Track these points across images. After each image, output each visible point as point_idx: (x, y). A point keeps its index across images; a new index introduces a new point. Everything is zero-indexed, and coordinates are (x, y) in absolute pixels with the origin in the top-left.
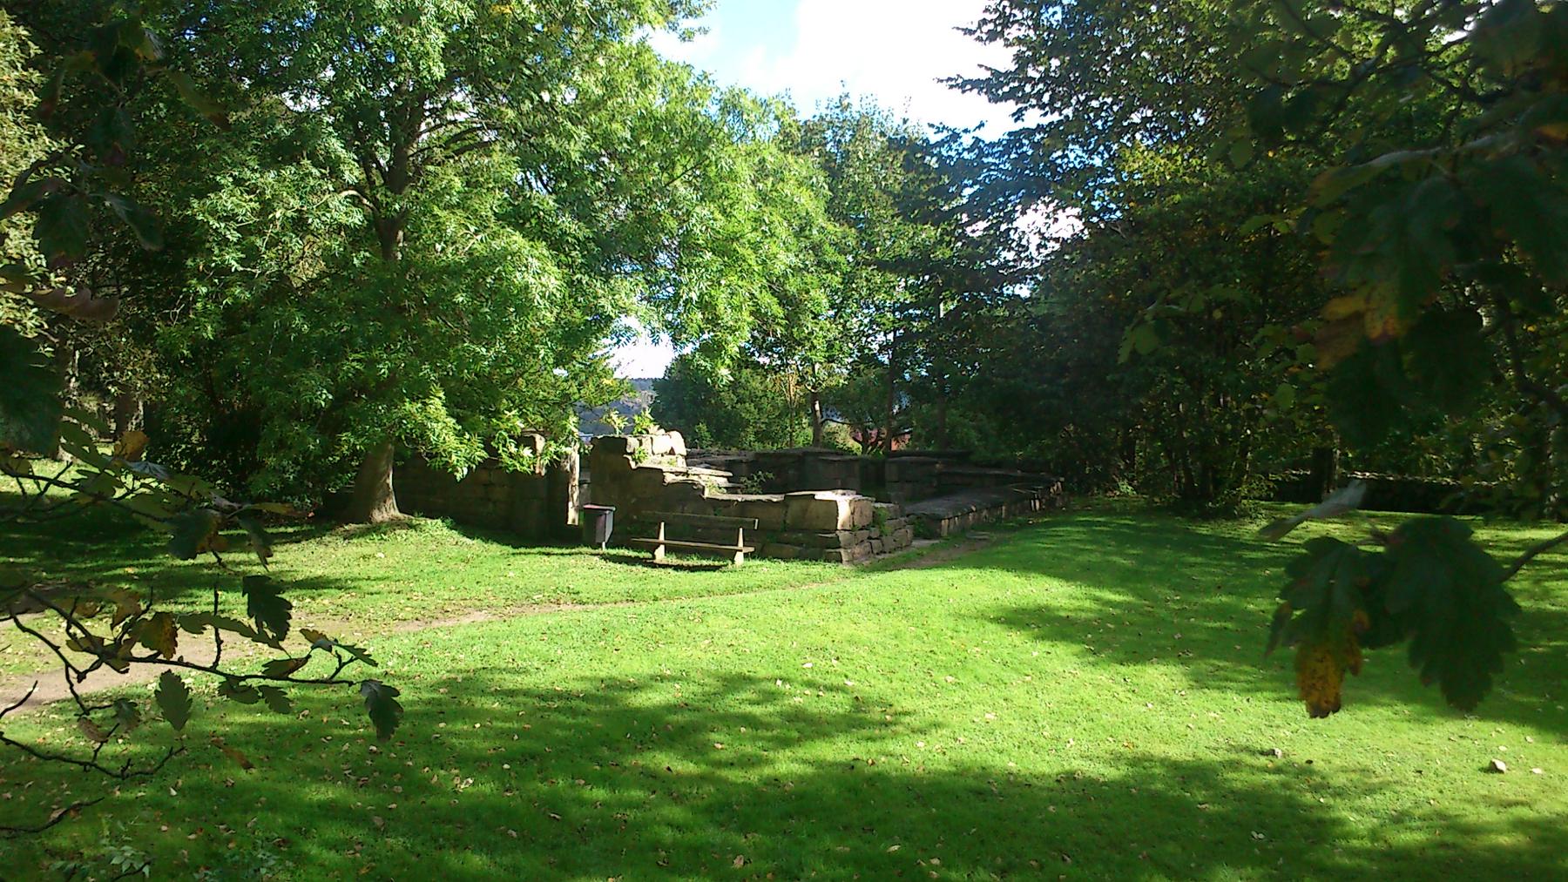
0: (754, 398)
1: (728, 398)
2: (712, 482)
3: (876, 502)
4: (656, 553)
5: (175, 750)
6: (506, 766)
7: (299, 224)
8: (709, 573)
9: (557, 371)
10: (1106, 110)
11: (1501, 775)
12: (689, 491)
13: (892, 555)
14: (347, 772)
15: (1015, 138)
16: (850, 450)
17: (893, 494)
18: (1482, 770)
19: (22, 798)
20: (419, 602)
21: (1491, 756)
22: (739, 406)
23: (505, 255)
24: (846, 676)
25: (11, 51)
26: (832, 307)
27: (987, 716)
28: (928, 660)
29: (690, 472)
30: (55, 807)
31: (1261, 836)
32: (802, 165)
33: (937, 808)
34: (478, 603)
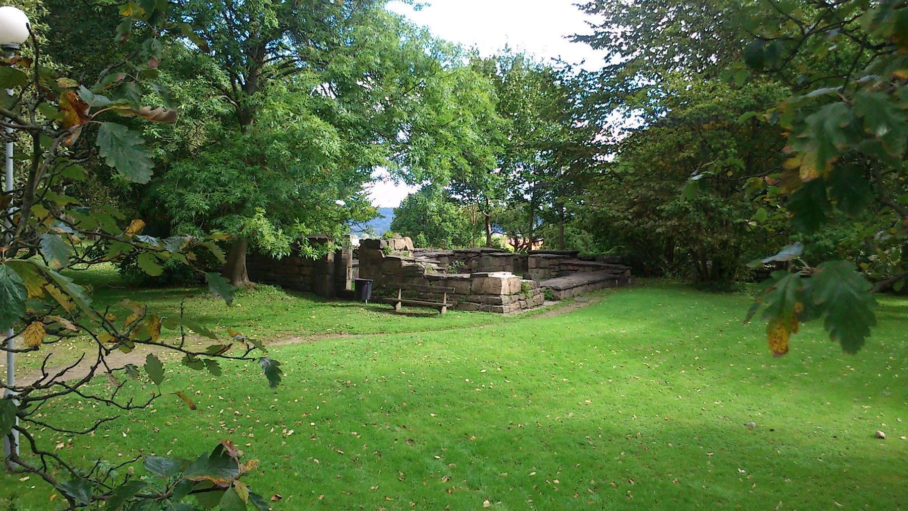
0: (452, 220)
1: (437, 219)
2: (430, 268)
3: (523, 279)
4: (396, 306)
5: (155, 396)
6: (313, 424)
7: (195, 113)
8: (426, 318)
9: (338, 202)
10: (659, 54)
11: (883, 440)
12: (414, 271)
13: (532, 310)
14: (223, 425)
15: (607, 71)
16: (507, 250)
17: (533, 275)
18: (871, 437)
19: (40, 437)
20: (262, 331)
21: (877, 429)
22: (443, 224)
23: (315, 132)
24: (506, 378)
25: (33, 12)
26: (499, 166)
27: (587, 401)
28: (553, 369)
29: (416, 260)
30: (58, 442)
31: (743, 471)
32: (481, 80)
33: (557, 452)
34: (295, 333)
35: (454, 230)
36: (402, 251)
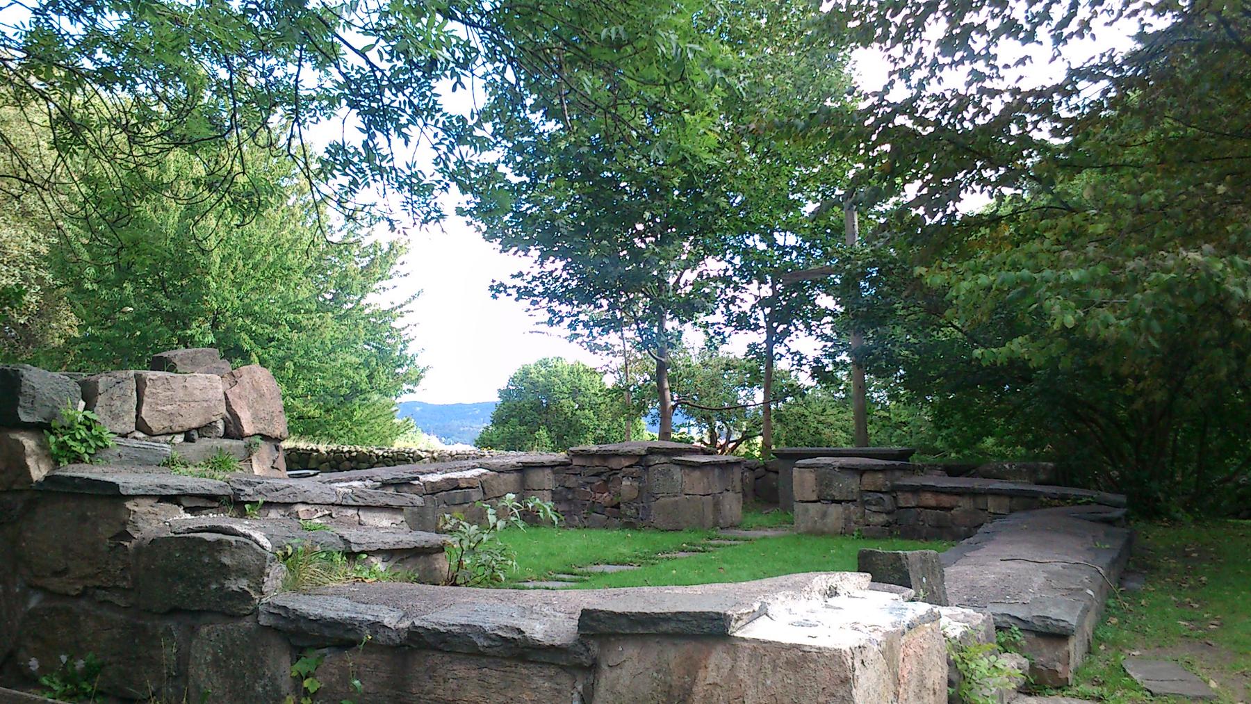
22: (578, 412)
35: (597, 423)
36: (203, 444)
